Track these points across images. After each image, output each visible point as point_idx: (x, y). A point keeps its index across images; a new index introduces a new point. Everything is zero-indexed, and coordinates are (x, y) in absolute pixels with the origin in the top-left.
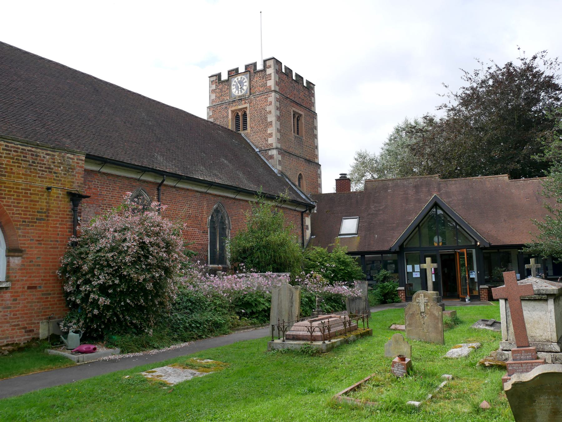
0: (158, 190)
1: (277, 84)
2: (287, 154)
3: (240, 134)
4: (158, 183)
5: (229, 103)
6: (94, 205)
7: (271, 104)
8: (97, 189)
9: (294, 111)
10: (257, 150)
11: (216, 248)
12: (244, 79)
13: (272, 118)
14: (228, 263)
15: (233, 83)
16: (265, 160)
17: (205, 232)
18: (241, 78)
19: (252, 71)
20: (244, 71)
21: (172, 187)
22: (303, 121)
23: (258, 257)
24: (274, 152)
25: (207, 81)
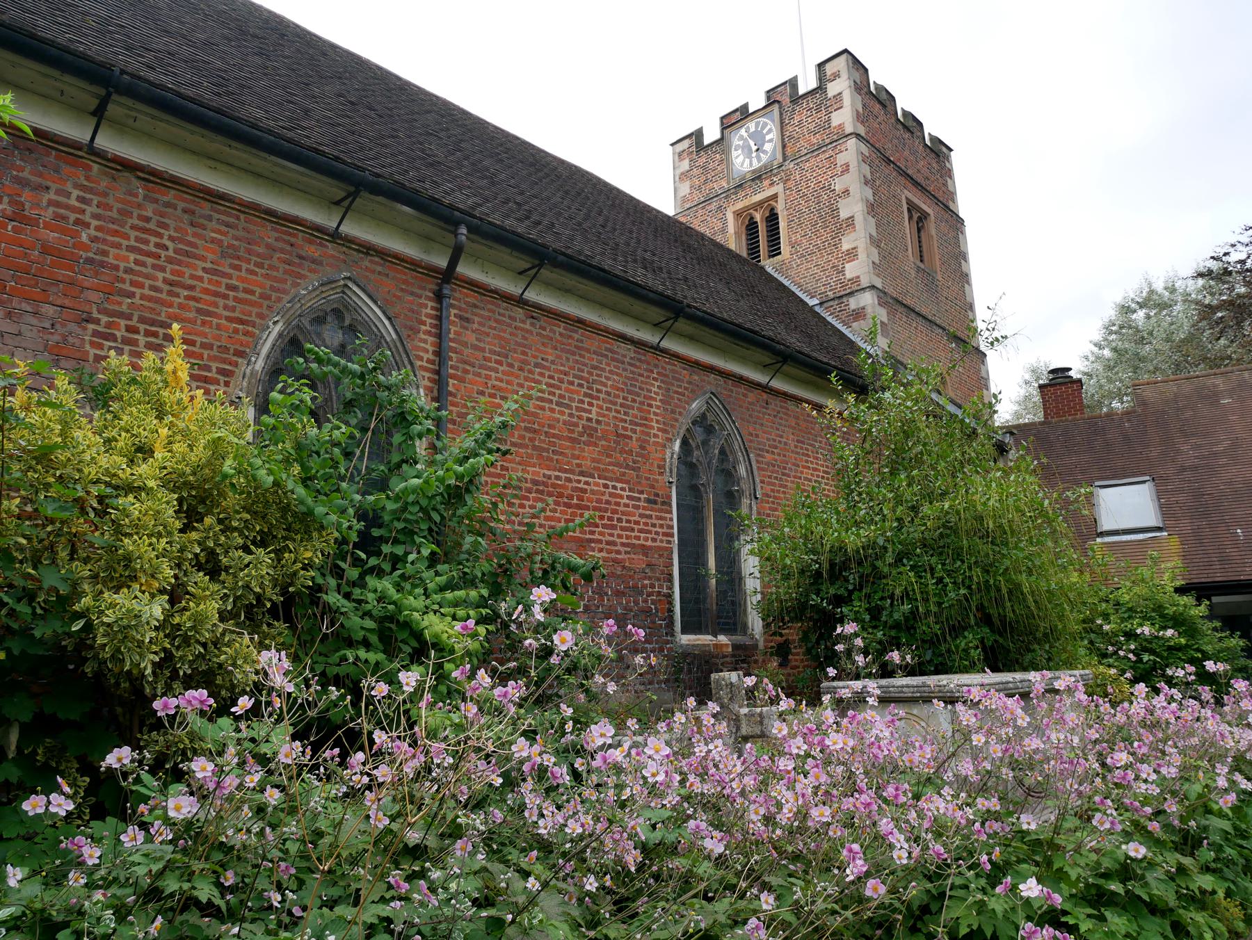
0: (439, 297)
1: (860, 118)
2: (901, 309)
3: (762, 268)
4: (433, 269)
5: (728, 194)
6: (48, 310)
8: (76, 235)
9: (909, 202)
10: (812, 302)
11: (705, 564)
12: (765, 124)
13: (853, 207)
14: (755, 623)
15: (736, 142)
16: (839, 326)
17: (657, 501)
18: (757, 125)
19: (786, 100)
20: (763, 103)
21: (506, 297)
22: (933, 232)
23: (906, 595)
25: (668, 154)
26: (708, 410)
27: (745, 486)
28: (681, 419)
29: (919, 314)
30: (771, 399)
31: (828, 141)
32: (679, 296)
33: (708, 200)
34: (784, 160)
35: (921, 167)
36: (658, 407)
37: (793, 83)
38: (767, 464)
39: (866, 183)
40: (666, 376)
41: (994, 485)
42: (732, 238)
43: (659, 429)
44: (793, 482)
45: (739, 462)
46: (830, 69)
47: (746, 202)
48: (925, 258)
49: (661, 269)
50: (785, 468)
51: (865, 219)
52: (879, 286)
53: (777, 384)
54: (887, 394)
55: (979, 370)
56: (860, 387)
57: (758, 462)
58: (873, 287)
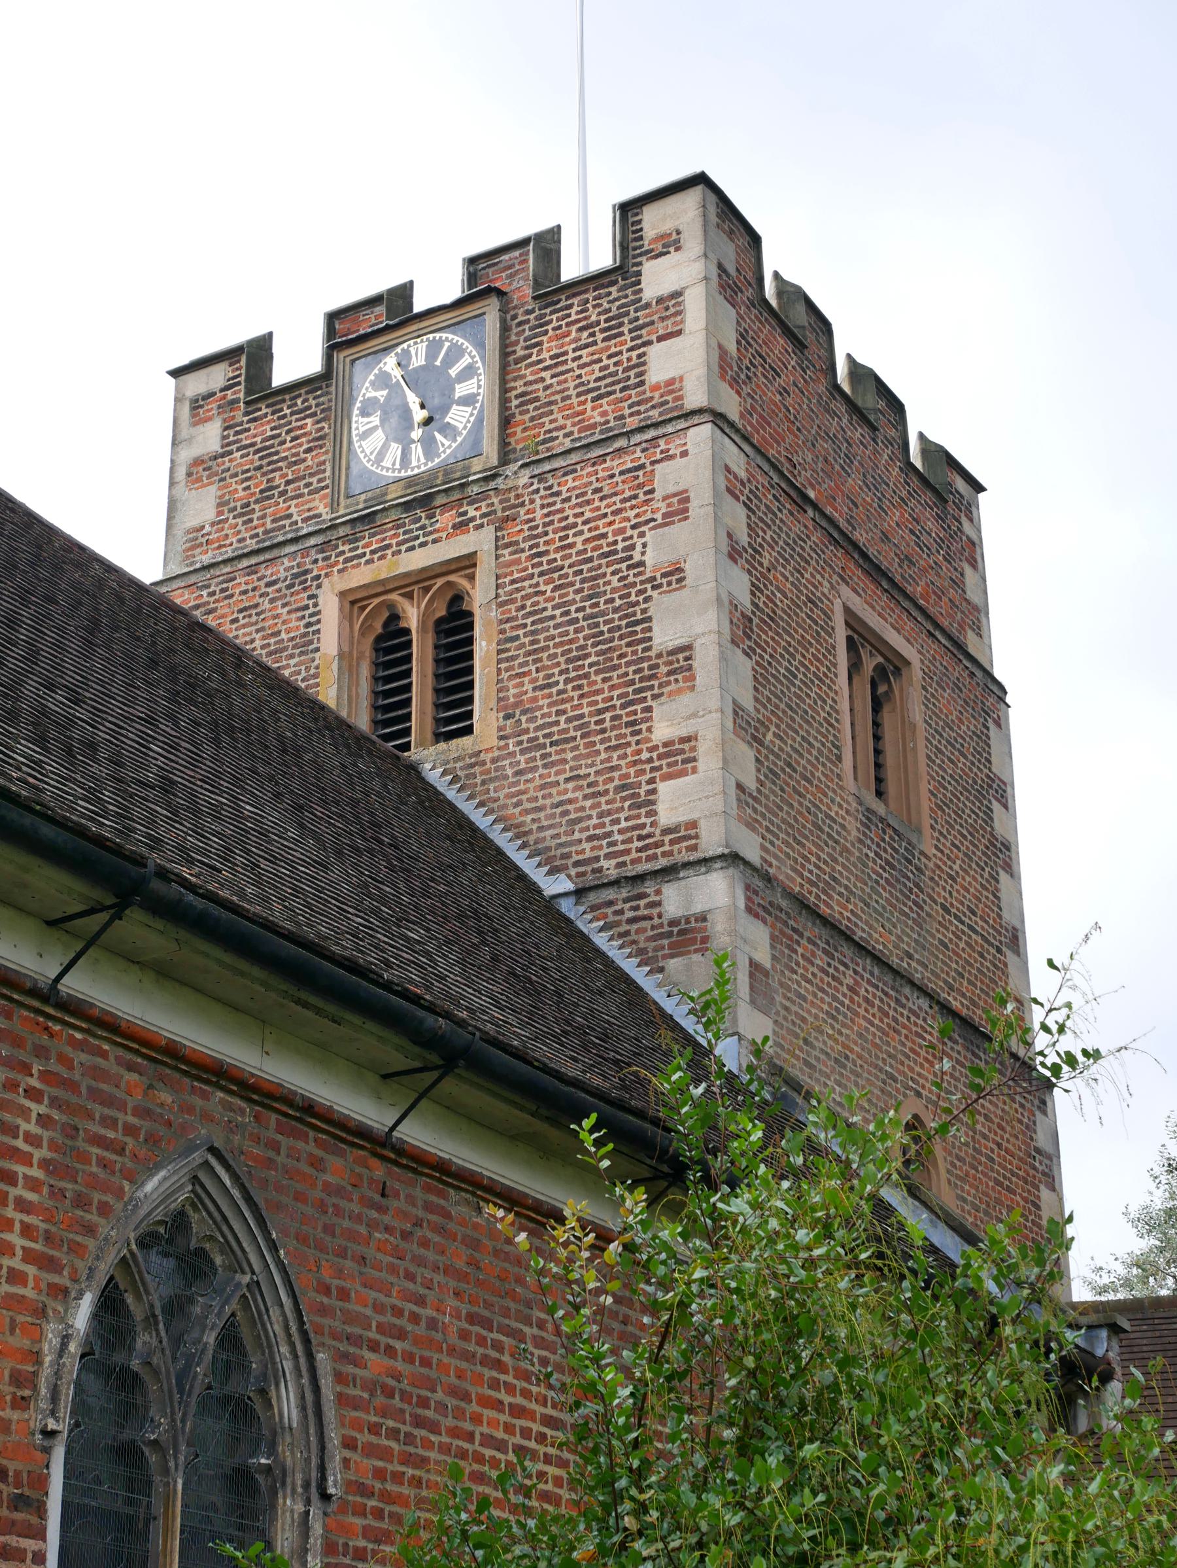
1: (728, 368)
2: (812, 930)
3: (413, 769)
5: (330, 538)
7: (679, 508)
9: (853, 621)
10: (554, 885)
12: (456, 353)
13: (689, 619)
15: (366, 389)
16: (629, 966)
19: (522, 289)
22: (917, 713)
24: (714, 894)
26: (196, 1202)
27: (291, 1455)
28: (104, 1228)
29: (862, 949)
30: (398, 1180)
31: (632, 422)
32: (137, 844)
33: (268, 550)
34: (504, 460)
35: (890, 527)
36: (33, 1185)
37: (547, 245)
38: (371, 1387)
39: (734, 554)
40: (72, 1086)
41: (1040, 1506)
42: (328, 670)
43: (29, 1256)
44: (445, 1449)
45: (278, 1376)
46: (653, 221)
47: (382, 570)
48: (891, 788)
49: (92, 746)
50: (424, 1403)
51: (723, 658)
52: (753, 855)
53: (418, 1134)
54: (739, 1205)
55: (1031, 1128)
56: (662, 1165)
57: (339, 1378)
58: (733, 859)
